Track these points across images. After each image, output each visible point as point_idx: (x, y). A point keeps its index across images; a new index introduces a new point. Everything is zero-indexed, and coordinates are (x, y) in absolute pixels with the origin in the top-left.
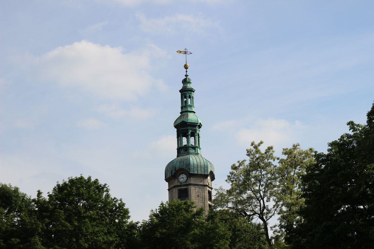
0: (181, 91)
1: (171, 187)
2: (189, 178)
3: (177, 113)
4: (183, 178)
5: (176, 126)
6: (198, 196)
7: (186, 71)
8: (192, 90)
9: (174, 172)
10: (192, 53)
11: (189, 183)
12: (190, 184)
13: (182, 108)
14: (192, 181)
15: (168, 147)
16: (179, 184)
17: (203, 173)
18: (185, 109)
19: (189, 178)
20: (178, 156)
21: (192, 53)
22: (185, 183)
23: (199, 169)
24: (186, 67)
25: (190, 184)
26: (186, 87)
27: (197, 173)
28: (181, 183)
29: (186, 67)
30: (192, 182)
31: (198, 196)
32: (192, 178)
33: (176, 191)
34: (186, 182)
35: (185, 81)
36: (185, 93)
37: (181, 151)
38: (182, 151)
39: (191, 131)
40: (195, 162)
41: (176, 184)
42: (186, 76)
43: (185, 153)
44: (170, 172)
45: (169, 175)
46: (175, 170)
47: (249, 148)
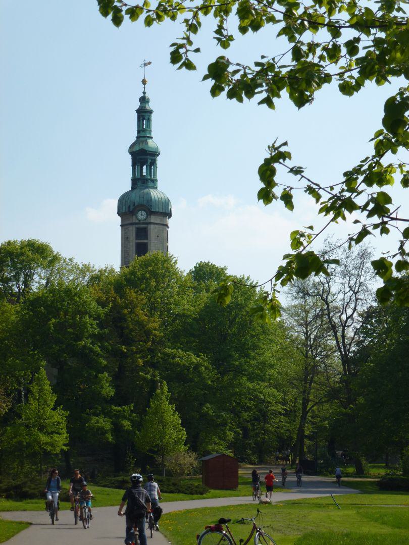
0: (138, 111)
1: (124, 223)
2: (149, 216)
3: (131, 136)
4: (141, 215)
5: (132, 153)
6: (158, 236)
7: (144, 88)
8: (151, 112)
9: (132, 208)
10: (150, 63)
11: (149, 221)
12: (151, 223)
13: (139, 132)
14: (153, 219)
15: (122, 181)
16: (137, 221)
17: (164, 211)
18: (143, 133)
19: (149, 216)
20: (133, 188)
21: (150, 63)
22: (144, 221)
23: (160, 206)
24: (144, 82)
25: (151, 223)
26: (145, 107)
27: (239, 481)
28: (139, 221)
29: (144, 82)
30: (152, 221)
31: (158, 236)
32: (152, 216)
33: (132, 230)
34: (145, 220)
35: (144, 100)
36: (143, 114)
37: (138, 183)
38: (139, 184)
39: (150, 161)
40: (156, 196)
41: (134, 221)
42: (144, 93)
43: (143, 186)
44: (127, 206)
45: (124, 210)
46: (134, 205)
47: (291, 104)
